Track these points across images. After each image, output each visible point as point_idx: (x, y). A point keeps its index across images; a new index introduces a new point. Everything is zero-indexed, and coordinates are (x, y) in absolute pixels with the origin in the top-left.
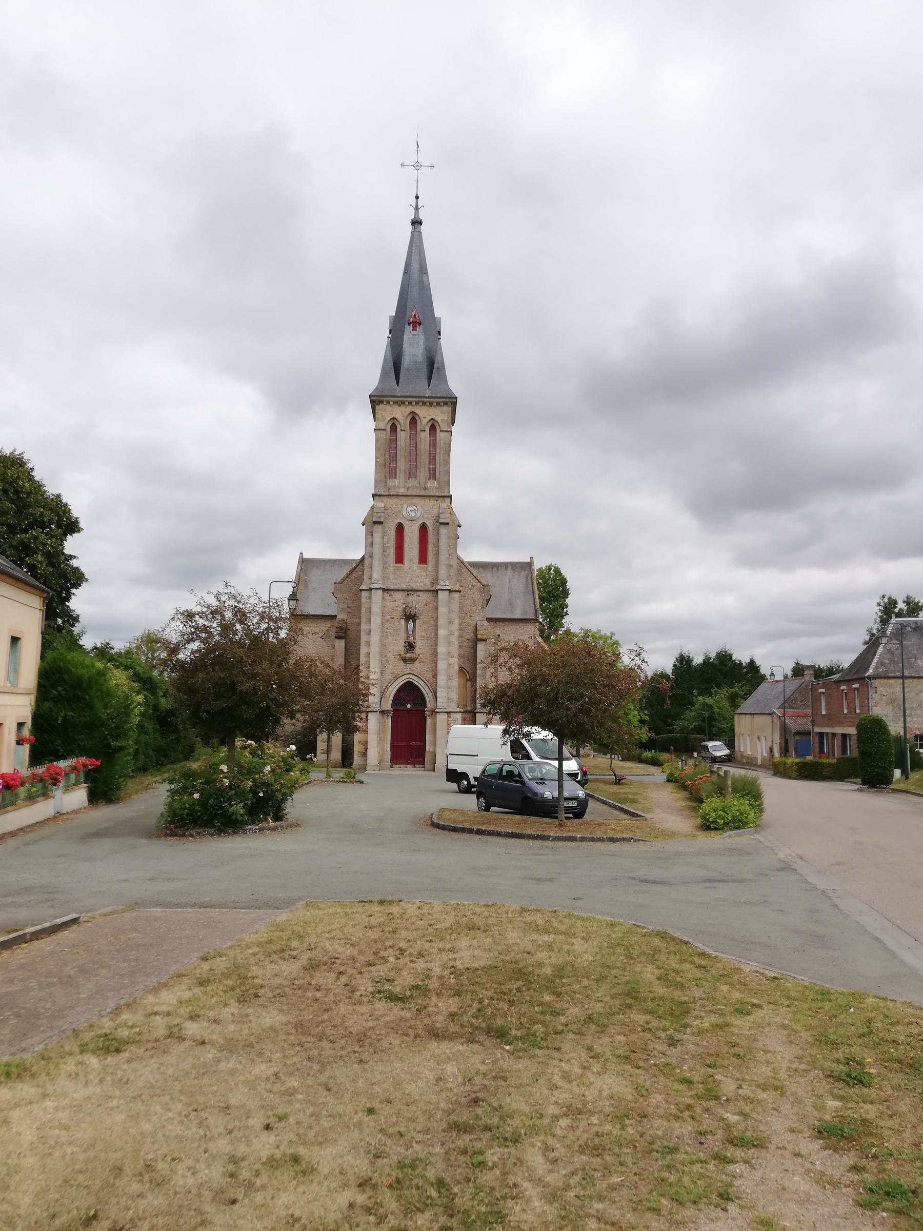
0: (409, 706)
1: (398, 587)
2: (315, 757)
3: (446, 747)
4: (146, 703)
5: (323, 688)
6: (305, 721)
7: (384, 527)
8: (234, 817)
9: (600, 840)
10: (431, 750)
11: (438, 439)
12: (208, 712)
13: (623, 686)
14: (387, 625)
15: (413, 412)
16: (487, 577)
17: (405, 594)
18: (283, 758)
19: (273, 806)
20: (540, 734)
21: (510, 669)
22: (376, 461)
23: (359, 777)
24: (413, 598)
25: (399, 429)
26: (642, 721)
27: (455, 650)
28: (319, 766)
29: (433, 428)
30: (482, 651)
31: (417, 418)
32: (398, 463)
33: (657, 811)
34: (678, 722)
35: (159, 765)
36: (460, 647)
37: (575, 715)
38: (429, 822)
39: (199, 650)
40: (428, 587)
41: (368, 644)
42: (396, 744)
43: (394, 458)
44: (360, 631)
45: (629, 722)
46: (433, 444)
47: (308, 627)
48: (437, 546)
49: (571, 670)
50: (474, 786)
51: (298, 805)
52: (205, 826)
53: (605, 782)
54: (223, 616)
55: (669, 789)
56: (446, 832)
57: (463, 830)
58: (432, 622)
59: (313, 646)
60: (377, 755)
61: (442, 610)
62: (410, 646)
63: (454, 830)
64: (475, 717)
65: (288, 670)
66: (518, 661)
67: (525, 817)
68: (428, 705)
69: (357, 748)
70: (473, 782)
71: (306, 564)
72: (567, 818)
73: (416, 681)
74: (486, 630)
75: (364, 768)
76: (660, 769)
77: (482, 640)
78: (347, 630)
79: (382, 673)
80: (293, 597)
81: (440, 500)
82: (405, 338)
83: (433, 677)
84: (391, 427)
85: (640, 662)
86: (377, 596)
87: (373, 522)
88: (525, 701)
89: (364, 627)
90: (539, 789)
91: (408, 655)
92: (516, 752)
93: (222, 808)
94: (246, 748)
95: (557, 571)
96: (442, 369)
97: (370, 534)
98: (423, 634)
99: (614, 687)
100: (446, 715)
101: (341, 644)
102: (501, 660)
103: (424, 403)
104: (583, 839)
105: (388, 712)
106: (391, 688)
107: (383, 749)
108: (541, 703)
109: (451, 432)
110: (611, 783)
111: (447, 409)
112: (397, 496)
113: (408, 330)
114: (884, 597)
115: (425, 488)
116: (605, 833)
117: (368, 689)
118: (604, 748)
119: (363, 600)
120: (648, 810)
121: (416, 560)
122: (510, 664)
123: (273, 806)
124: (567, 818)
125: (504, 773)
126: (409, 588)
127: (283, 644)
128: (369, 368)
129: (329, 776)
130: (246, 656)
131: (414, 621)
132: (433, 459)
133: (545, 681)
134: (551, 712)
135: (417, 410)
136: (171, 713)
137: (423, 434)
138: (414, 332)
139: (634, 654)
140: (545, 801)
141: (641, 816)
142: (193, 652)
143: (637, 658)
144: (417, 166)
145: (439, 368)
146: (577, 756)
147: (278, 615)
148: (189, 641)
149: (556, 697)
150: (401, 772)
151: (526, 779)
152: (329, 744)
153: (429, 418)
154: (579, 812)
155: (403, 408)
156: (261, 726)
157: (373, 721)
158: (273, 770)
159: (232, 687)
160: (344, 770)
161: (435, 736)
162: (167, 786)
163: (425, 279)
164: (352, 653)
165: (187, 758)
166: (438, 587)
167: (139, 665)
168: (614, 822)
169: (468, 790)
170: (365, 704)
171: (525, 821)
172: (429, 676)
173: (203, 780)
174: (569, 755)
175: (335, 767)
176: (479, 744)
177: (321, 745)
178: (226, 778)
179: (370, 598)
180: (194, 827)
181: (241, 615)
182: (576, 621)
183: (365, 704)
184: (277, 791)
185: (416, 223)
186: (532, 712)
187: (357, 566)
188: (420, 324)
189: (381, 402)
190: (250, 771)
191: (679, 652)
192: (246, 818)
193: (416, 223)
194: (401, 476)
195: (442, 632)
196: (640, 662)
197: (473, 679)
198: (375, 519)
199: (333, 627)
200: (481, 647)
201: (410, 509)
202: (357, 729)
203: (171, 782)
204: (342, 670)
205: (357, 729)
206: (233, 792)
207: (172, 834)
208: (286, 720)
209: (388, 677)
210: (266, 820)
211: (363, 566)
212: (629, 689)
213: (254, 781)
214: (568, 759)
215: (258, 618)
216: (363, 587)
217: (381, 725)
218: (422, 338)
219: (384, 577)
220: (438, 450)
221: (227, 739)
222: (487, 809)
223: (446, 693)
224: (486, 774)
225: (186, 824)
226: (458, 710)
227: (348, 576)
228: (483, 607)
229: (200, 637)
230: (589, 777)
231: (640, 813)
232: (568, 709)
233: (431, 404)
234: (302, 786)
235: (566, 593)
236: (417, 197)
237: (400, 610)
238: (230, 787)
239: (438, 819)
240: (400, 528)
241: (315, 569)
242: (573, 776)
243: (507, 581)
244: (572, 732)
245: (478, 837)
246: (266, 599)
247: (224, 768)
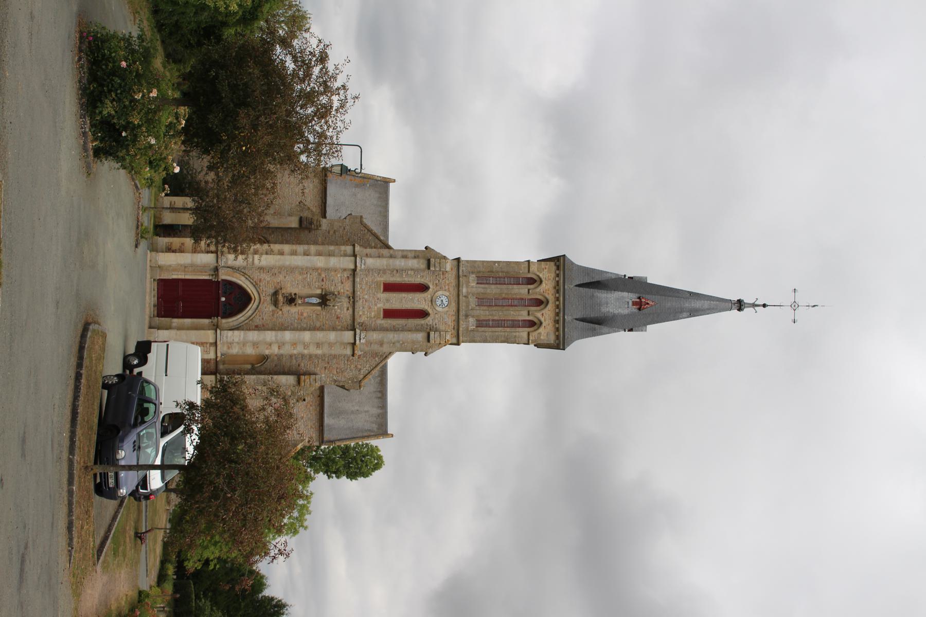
0: (223, 299)
1: (358, 286)
2: (166, 195)
3: (176, 340)
4: (229, 14)
5: (242, 202)
6: (207, 182)
7: (423, 271)
8: (99, 104)
9: (70, 512)
10: (174, 325)
11: (521, 329)
12: (216, 77)
13: (246, 536)
14: (315, 274)
15: (548, 302)
16: (370, 385)
17: (350, 293)
18: (165, 158)
19: (111, 147)
20: (191, 443)
21: (264, 409)
22: (495, 262)
23: (143, 244)
24: (345, 303)
26: (207, 562)
27: (287, 350)
28: (157, 200)
29: (532, 324)
30: (287, 381)
31: (542, 306)
32: (493, 286)
33: (105, 578)
34: (208, 603)
35: (160, 27)
36: (291, 356)
37: (211, 483)
38: (91, 320)
39: (285, 68)
40: (358, 320)
41: (294, 253)
43: (499, 281)
44: (308, 244)
45: (206, 548)
46: (515, 324)
47: (311, 186)
48: (403, 329)
49: (262, 478)
50: (131, 372)
51: (111, 174)
52: (90, 74)
53: (138, 521)
54: (322, 94)
55: (130, 593)
56: (78, 339)
57: (80, 358)
58: (318, 324)
59: (289, 193)
60: (168, 263)
61: (332, 336)
62: (291, 300)
63: (81, 348)
64: (211, 373)
65: (262, 163)
66: (273, 418)
67: (95, 427)
68: (224, 321)
69: (176, 241)
70: (136, 371)
72: (95, 475)
73: (252, 306)
74: (310, 386)
75: (154, 249)
76: (154, 583)
77: (299, 382)
78: (310, 230)
79: (261, 269)
80: (344, 170)
81: (454, 332)
82: (625, 294)
83: (256, 326)
84: (531, 278)
85: (272, 554)
86: (348, 263)
87: (429, 258)
88: (226, 427)
89: (313, 248)
90: (128, 444)
91: (281, 298)
92: (170, 418)
93: (110, 91)
94: (177, 118)
95: (377, 466)
96: (594, 333)
97: (416, 255)
98: (305, 315)
99: (244, 526)
100: (212, 340)
101: (294, 223)
102: (274, 400)
103: (557, 314)
104: (70, 493)
105: (217, 275)
106: (243, 278)
107: (175, 270)
108: (224, 444)
109: (528, 344)
110: (136, 528)
111: (552, 339)
112: (458, 286)
113: (633, 297)
115: (467, 316)
116: (78, 518)
117: (242, 253)
118: (178, 521)
119: (343, 248)
120: (105, 568)
122: (269, 409)
123: (111, 147)
124: (95, 475)
125: (146, 405)
126: (357, 299)
127: (291, 158)
128: (590, 255)
129: (145, 209)
130: (278, 119)
131: (319, 304)
132: (499, 324)
133: (250, 447)
134: (214, 455)
135: (551, 306)
136: (219, 39)
137: (525, 313)
138: (631, 303)
139: (282, 548)
140: (114, 452)
141: (98, 559)
142: (283, 62)
143: (277, 552)
144: (795, 306)
145: (595, 329)
146: (167, 488)
147: (324, 152)
148: (295, 60)
149: (231, 461)
150: (148, 290)
151: (139, 429)
152: (181, 210)
153: (542, 320)
154: (102, 489)
155: (552, 291)
156: (200, 135)
157: (207, 259)
158: (151, 146)
159: (243, 103)
160: (152, 227)
161: (188, 329)
162: (135, 34)
163: (685, 314)
164: (284, 235)
165: (168, 56)
166: (358, 331)
167: (270, 8)
168: (91, 529)
169: (127, 365)
170: (225, 249)
171: (91, 428)
172: (258, 321)
173: (141, 72)
174: (168, 478)
175: (155, 217)
176: (179, 373)
177: (179, 201)
178: (143, 96)
179: (345, 255)
180: (89, 61)
181: (324, 112)
182: (322, 488)
183: (225, 249)
184: (128, 151)
185: (740, 305)
186: (215, 434)
187: (380, 241)
188: (639, 309)
189: (558, 268)
190: (150, 121)
191: (289, 603)
192: (98, 118)
193: (740, 305)
194: (481, 289)
195: (307, 336)
196: (272, 554)
197: (253, 371)
198: (432, 260)
199: (313, 214)
200: (290, 380)
202: (197, 240)
203: (140, 37)
204: (262, 225)
205: (197, 240)
206: (127, 103)
207: (82, 38)
208: (206, 161)
209: (256, 275)
210: (95, 139)
211: (381, 248)
212: (242, 543)
213: (139, 126)
214: (163, 478)
215: (320, 130)
216: (357, 248)
217: (202, 268)
218: (624, 311)
219: (368, 271)
220: (508, 329)
221: (187, 98)
222: (105, 386)
223: (238, 340)
224: (145, 384)
225: (92, 52)
226: (219, 355)
227: (370, 231)
228: (335, 381)
229: (299, 70)
230: (144, 502)
231: (102, 558)
232: (218, 475)
233: (557, 322)
234: (133, 180)
235: (352, 476)
236: (764, 306)
237: (332, 289)
238: (133, 100)
239: (94, 330)
240: (423, 288)
241: (377, 195)
242: (144, 483)
243: (366, 409)
244: (192, 480)
245: (73, 376)
246: (342, 141)
247: (154, 93)
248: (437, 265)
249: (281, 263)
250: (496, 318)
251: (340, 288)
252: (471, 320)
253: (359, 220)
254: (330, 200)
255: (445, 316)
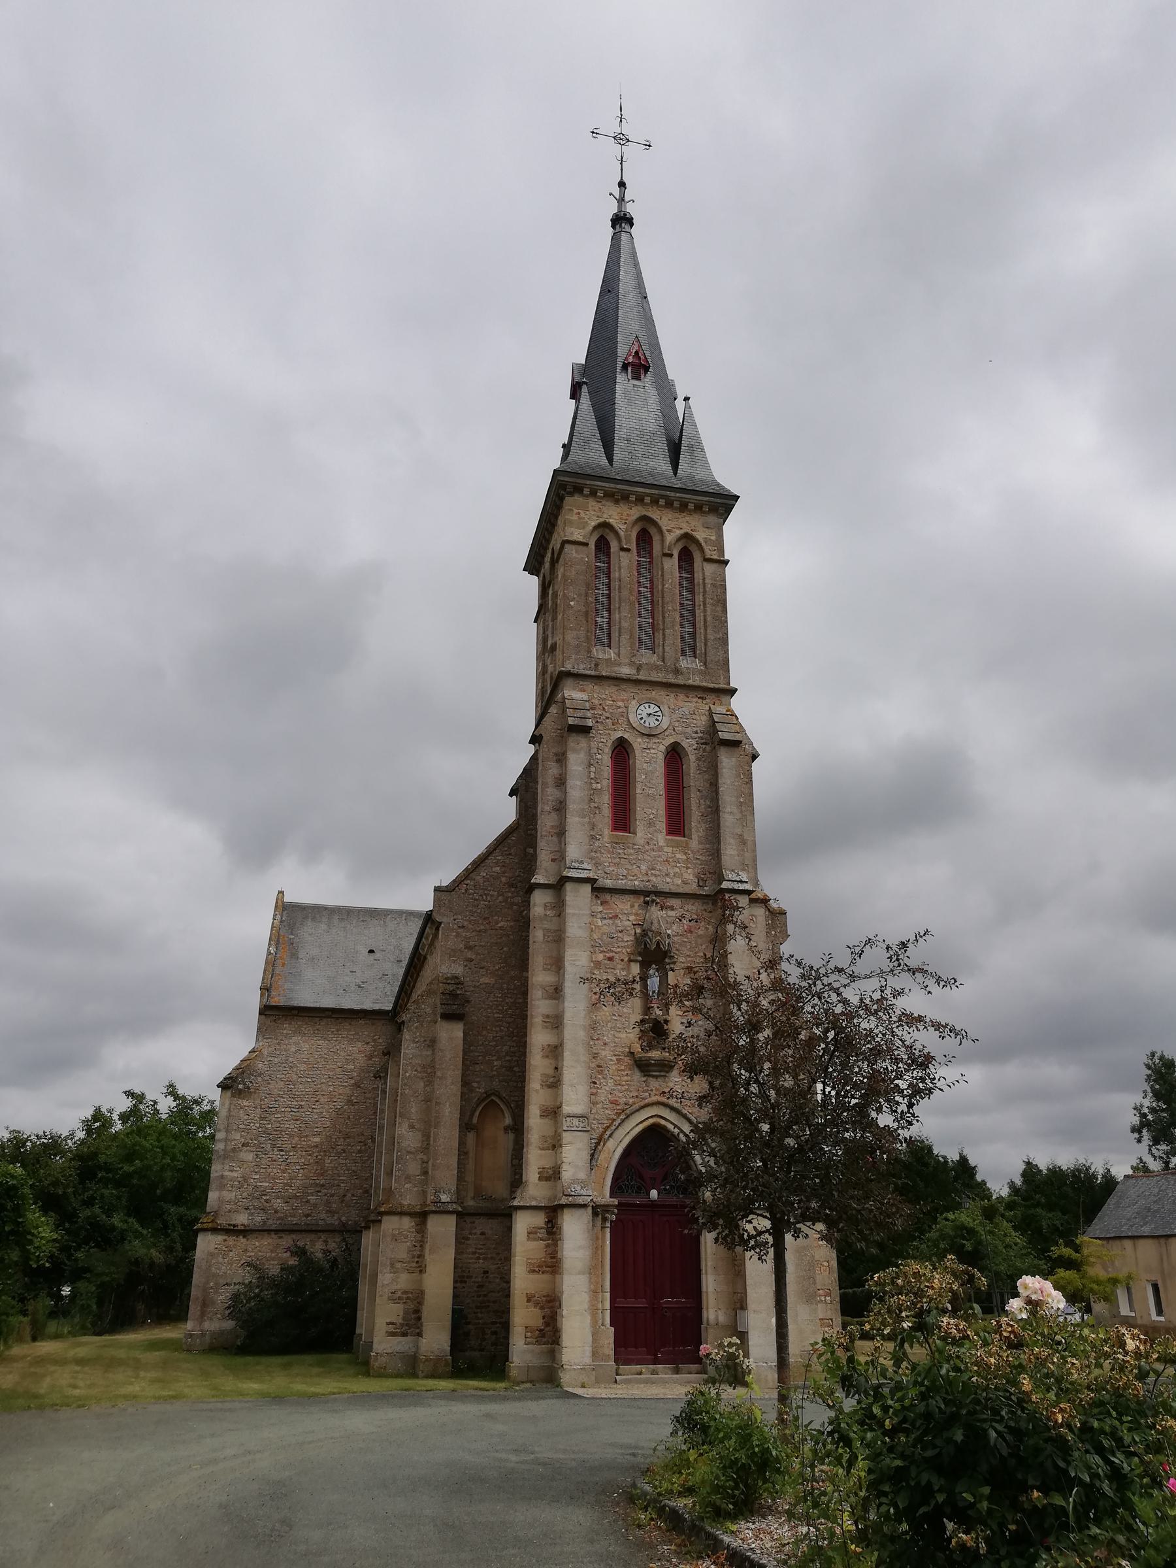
0: (654, 1194)
1: (621, 883)
11: (698, 576)
25: (614, 546)
32: (616, 616)
40: (692, 888)
41: (556, 1022)
42: (622, 1302)
46: (689, 585)
71: (290, 917)
81: (710, 698)
84: (597, 544)
96: (697, 447)
106: (611, 1144)
112: (617, 680)
114: (1153, 1054)
115: (677, 671)
121: (662, 825)
126: (650, 887)
132: (689, 616)
135: (654, 514)
144: (622, 139)
153: (678, 532)
155: (623, 508)
185: (621, 221)
189: (578, 489)
201: (645, 710)
209: (605, 1113)
216: (539, 878)
219: (592, 854)
220: (699, 598)
236: (622, 184)
237: (629, 938)
241: (309, 923)
248: (580, 714)
249: (581, 1050)
250: (678, 619)
251: (626, 923)
252: (685, 663)
253: (444, 896)
254: (328, 1002)
255: (679, 712)
